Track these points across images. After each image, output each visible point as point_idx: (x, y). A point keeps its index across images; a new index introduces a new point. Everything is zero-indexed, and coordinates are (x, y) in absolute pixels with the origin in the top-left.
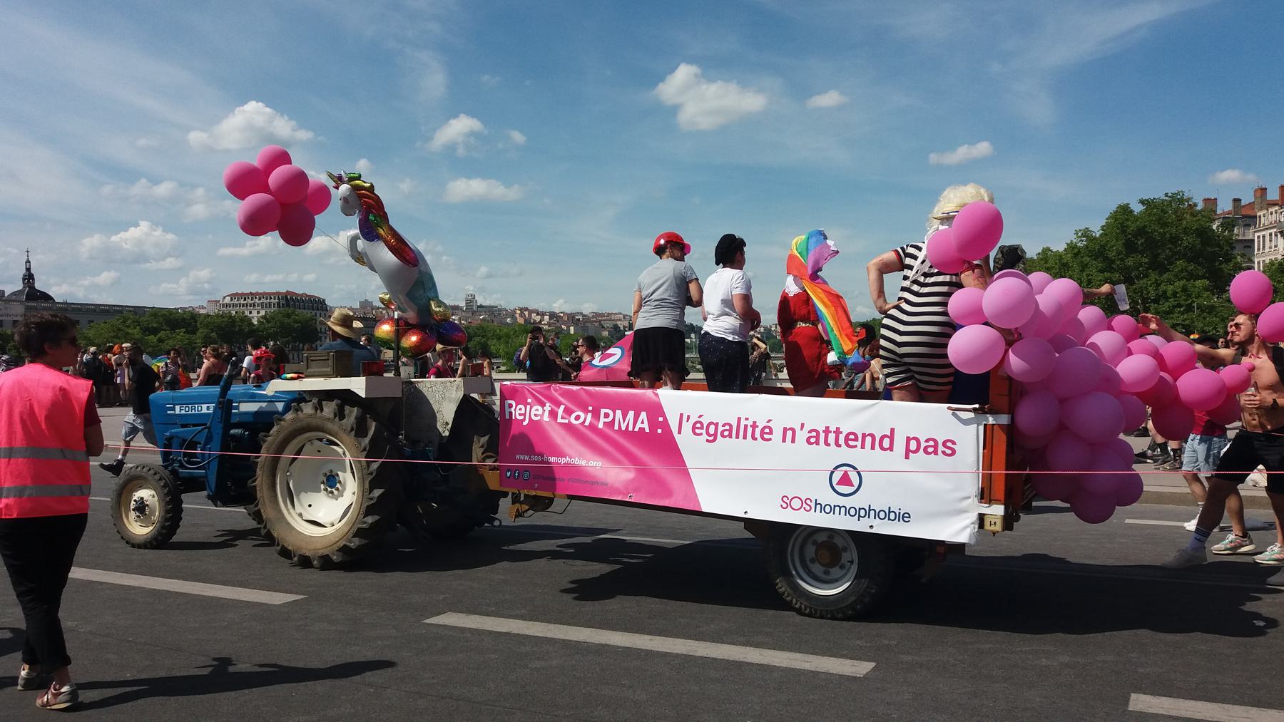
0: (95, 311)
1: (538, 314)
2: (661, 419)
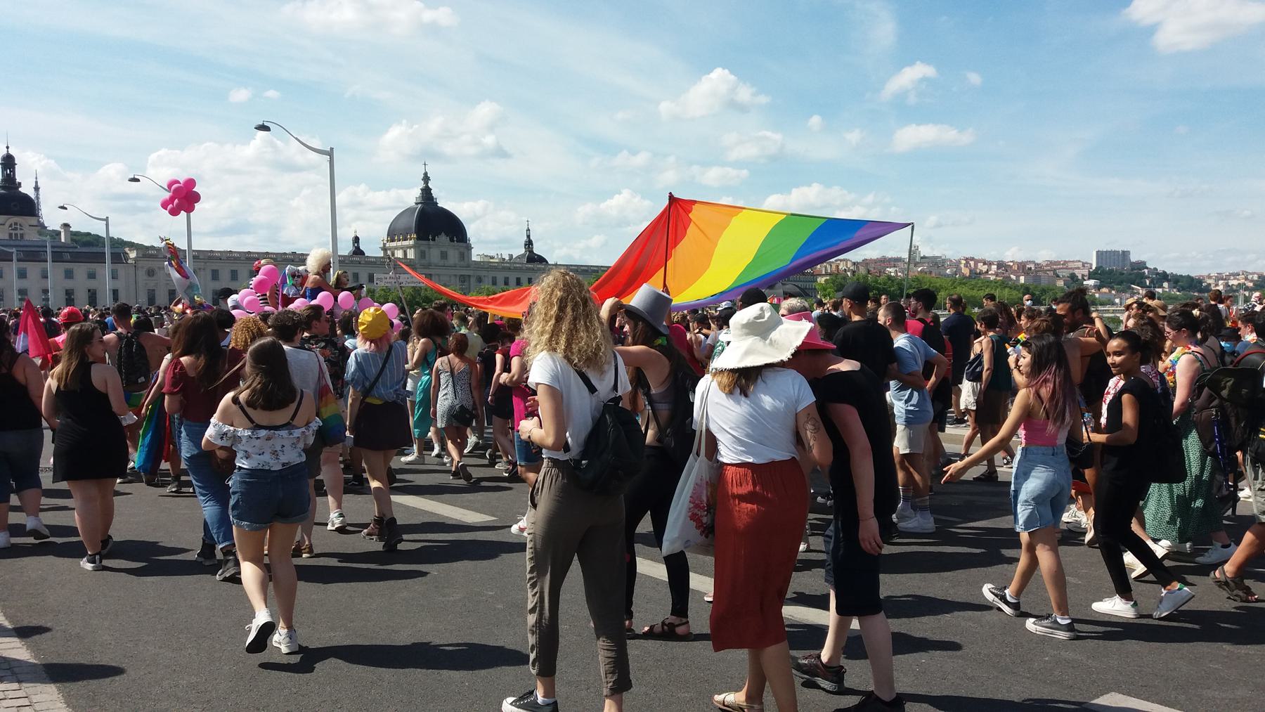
0: (510, 269)
1: (985, 264)
2: (133, 255)
